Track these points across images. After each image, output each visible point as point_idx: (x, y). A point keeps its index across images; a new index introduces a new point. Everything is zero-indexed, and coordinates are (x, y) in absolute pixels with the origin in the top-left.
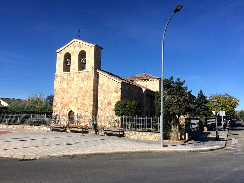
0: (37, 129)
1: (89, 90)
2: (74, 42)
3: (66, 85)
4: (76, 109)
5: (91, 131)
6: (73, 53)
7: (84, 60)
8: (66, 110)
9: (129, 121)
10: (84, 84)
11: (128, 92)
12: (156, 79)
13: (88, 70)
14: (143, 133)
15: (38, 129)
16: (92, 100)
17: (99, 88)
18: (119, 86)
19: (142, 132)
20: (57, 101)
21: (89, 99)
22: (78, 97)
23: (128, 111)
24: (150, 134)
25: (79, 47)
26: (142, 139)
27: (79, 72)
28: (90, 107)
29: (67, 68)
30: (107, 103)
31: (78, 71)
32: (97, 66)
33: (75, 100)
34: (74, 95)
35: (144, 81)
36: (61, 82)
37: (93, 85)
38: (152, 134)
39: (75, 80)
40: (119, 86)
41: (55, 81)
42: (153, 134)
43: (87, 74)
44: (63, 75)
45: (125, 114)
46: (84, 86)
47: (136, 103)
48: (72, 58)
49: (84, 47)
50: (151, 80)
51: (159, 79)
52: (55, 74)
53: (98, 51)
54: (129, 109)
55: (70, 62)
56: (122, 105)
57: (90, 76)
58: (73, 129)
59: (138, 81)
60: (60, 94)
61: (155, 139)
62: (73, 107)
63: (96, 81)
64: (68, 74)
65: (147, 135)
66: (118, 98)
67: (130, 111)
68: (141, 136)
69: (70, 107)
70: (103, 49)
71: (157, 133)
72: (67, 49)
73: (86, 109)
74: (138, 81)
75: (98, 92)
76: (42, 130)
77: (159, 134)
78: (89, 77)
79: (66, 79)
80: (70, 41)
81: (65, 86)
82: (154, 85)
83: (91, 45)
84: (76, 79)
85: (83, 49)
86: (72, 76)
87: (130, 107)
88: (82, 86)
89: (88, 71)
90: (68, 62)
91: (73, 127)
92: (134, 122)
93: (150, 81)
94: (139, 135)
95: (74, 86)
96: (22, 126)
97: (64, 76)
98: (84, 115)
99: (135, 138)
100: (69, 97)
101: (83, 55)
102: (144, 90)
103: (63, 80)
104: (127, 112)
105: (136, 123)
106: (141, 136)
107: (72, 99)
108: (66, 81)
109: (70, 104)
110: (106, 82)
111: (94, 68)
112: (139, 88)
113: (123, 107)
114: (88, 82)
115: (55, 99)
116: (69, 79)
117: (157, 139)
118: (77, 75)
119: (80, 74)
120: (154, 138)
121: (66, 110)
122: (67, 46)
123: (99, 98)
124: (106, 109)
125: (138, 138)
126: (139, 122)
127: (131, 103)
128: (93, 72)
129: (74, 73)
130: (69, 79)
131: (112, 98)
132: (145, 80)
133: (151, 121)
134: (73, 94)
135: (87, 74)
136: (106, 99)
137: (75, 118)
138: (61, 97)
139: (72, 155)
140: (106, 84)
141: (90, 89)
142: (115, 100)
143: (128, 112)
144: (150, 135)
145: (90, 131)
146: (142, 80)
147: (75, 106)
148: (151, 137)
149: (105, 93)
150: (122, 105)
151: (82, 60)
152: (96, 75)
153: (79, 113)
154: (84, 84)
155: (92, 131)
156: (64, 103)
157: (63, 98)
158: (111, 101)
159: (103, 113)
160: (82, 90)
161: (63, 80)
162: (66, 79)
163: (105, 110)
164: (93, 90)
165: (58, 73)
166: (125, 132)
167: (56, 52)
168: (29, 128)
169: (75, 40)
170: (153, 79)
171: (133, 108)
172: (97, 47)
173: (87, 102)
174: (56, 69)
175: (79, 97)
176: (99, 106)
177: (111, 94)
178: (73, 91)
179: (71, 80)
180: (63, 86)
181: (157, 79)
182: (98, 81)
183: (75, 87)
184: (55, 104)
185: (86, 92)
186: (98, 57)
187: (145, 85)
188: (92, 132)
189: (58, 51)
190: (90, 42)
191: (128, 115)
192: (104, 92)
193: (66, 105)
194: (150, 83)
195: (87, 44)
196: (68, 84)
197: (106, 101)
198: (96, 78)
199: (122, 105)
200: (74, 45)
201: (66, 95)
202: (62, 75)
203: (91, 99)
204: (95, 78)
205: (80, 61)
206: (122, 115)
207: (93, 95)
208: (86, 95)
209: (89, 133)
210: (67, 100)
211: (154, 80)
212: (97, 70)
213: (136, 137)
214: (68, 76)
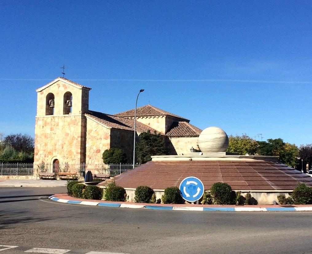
0: (25, 178)
1: (76, 137)
2: (58, 81)
3: (50, 130)
5: (81, 179)
6: (58, 94)
7: (70, 102)
9: (115, 168)
10: (70, 129)
11: (119, 138)
15: (26, 178)
16: (80, 147)
20: (39, 149)
25: (64, 88)
27: (65, 116)
28: (78, 155)
29: (50, 111)
31: (64, 114)
32: (85, 110)
33: (60, 147)
35: (147, 117)
36: (43, 127)
40: (109, 132)
41: (36, 125)
43: (74, 119)
44: (45, 118)
45: (112, 162)
46: (71, 132)
47: (122, 151)
48: (56, 99)
49: (69, 87)
50: (155, 116)
52: (36, 117)
53: (85, 92)
54: (115, 157)
55: (54, 104)
56: (109, 153)
57: (77, 121)
58: (63, 177)
59: (138, 118)
69: (54, 156)
70: (91, 89)
72: (50, 88)
75: (86, 139)
81: (47, 130)
82: (159, 123)
84: (61, 124)
86: (56, 120)
88: (68, 131)
89: (75, 115)
91: (62, 175)
93: (154, 118)
95: (59, 131)
96: (7, 176)
97: (47, 120)
98: (71, 163)
101: (68, 96)
103: (46, 124)
104: (114, 160)
107: (57, 146)
109: (55, 152)
111: (81, 112)
113: (110, 155)
114: (74, 127)
116: (53, 123)
119: (66, 118)
122: (50, 86)
123: (87, 145)
124: (95, 158)
127: (118, 151)
128: (81, 116)
130: (53, 123)
131: (101, 146)
132: (147, 116)
134: (58, 141)
135: (74, 119)
137: (62, 167)
138: (44, 144)
140: (94, 130)
141: (77, 135)
142: (104, 147)
145: (80, 178)
146: (143, 117)
152: (84, 120)
153: (66, 161)
156: (47, 151)
157: (46, 145)
158: (100, 149)
161: (46, 124)
164: (80, 137)
165: (40, 116)
168: (16, 177)
169: (59, 79)
170: (157, 115)
171: (120, 156)
172: (85, 89)
174: (37, 112)
175: (65, 144)
176: (87, 153)
177: (100, 141)
178: (57, 137)
179: (56, 125)
182: (86, 126)
185: (73, 138)
186: (86, 99)
187: (148, 124)
189: (40, 90)
193: (50, 153)
194: (153, 121)
196: (52, 129)
197: (95, 148)
198: (84, 123)
199: (110, 154)
200: (57, 85)
201: (49, 141)
205: (65, 102)
206: (109, 163)
207: (81, 142)
208: (73, 142)
210: (51, 147)
211: (158, 117)
212: (84, 114)
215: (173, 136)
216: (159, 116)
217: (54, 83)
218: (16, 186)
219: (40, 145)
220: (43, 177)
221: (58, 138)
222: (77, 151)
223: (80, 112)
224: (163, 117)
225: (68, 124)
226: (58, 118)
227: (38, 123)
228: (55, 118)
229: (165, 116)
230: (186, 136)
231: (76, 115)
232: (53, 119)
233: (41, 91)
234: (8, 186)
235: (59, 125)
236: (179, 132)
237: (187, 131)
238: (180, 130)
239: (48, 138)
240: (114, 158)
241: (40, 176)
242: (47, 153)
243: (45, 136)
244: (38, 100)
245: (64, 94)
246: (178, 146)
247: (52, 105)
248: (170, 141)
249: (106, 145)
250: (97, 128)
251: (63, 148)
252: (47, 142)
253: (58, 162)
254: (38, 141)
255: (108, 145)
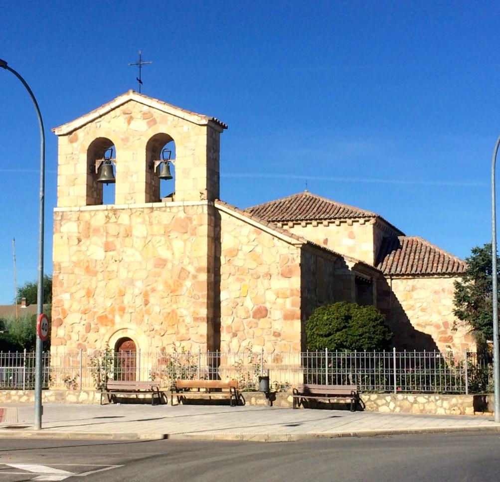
1: (191, 269)
2: (127, 102)
4: (145, 332)
5: (253, 400)
6: (126, 140)
8: (104, 335)
10: (170, 248)
12: (360, 217)
13: (183, 200)
14: (418, 396)
17: (223, 260)
18: (295, 256)
19: (415, 396)
20: (66, 306)
21: (194, 300)
22: (149, 293)
23: (358, 337)
24: (437, 398)
25: (148, 123)
26: (414, 412)
27: (152, 208)
30: (253, 312)
31: (147, 202)
33: (139, 301)
34: (134, 285)
35: (318, 223)
36: (79, 241)
37: (206, 252)
38: (443, 400)
39: (135, 232)
42: (447, 399)
43: (182, 215)
49: (164, 121)
50: (342, 220)
51: (374, 217)
52: (55, 209)
57: (195, 223)
59: (294, 224)
60: (78, 281)
61: (454, 412)
62: (132, 326)
63: (215, 239)
64: (106, 213)
65: (429, 402)
66: (292, 295)
67: (365, 338)
68: (412, 404)
69: (117, 327)
70: (227, 128)
71: (458, 396)
72: (98, 125)
73: (183, 331)
74: (294, 224)
76: (71, 403)
77: (463, 398)
78: (190, 226)
79: (102, 230)
80: (112, 99)
81: (95, 250)
83: (195, 118)
84: (139, 230)
85: (162, 129)
86: (124, 218)
87: (365, 326)
88: (164, 253)
89: (186, 204)
90: (100, 168)
92: (387, 367)
93: (340, 225)
94: (406, 404)
95: (132, 254)
99: (394, 411)
100: (114, 292)
102: (350, 265)
103: (88, 231)
105: (395, 369)
106: (412, 404)
107: (127, 299)
108: (102, 236)
110: (247, 241)
112: (334, 259)
114: (185, 241)
115: (58, 298)
116: (113, 229)
117: (458, 412)
118: (144, 218)
119: (156, 213)
120: (449, 409)
121: (104, 335)
122: (101, 116)
123: (223, 296)
125: (404, 411)
126: (403, 367)
128: (206, 208)
129: (131, 209)
131: (270, 296)
132: (321, 219)
133: (437, 363)
134: (132, 282)
135: (182, 215)
136: (248, 298)
138: (83, 293)
139: (352, 434)
141: (196, 265)
142: (280, 301)
143: (360, 339)
144: (437, 400)
146: (309, 221)
147: (140, 322)
148: (442, 407)
149: (244, 280)
150: (337, 319)
151: (155, 166)
154: (172, 249)
155: (257, 398)
156: (95, 313)
157: (89, 294)
158: (268, 306)
159: (238, 345)
160: (163, 268)
162: (99, 229)
163: (248, 333)
164: (206, 271)
166: (364, 397)
167: (57, 133)
168: (20, 397)
169: (131, 95)
170: (350, 218)
171: (374, 327)
173: (185, 309)
175: (153, 290)
176: (225, 320)
177: (266, 282)
180: (88, 253)
181: (367, 219)
183: (139, 258)
184: (61, 317)
185: (182, 274)
188: (256, 400)
189: (65, 129)
190: (191, 110)
191: (360, 349)
192: (241, 277)
193: (104, 320)
194: (338, 233)
195: (179, 113)
196: (108, 247)
197: (249, 304)
199: (340, 320)
200: (125, 113)
202: (82, 214)
203: (201, 300)
204: (88, 198)
208: (181, 285)
209: (247, 403)
210: (109, 303)
211: (353, 222)
213: (398, 409)
214: (109, 218)
215: (397, 275)
216: (355, 218)
217: (114, 109)
218: (143, 437)
219: (72, 294)
220: (119, 395)
221: (131, 275)
222: (194, 312)
223: (202, 194)
224: (366, 221)
225: (163, 232)
226: (129, 212)
227: (62, 228)
228: (118, 213)
229: (373, 221)
230: (439, 274)
231: (190, 203)
232: (113, 216)
233: (70, 133)
234: (111, 438)
235: (134, 232)
236: (411, 263)
237: (436, 262)
238: (412, 257)
239: (95, 273)
240: (357, 333)
241: (108, 390)
242: (96, 321)
243: (88, 267)
244: (61, 160)
245: (147, 140)
246: (412, 302)
247: (105, 174)
248: (390, 288)
249: (288, 293)
250: (255, 243)
251: (146, 303)
252: (94, 286)
253: (133, 347)
254: (62, 284)
255: (292, 295)
